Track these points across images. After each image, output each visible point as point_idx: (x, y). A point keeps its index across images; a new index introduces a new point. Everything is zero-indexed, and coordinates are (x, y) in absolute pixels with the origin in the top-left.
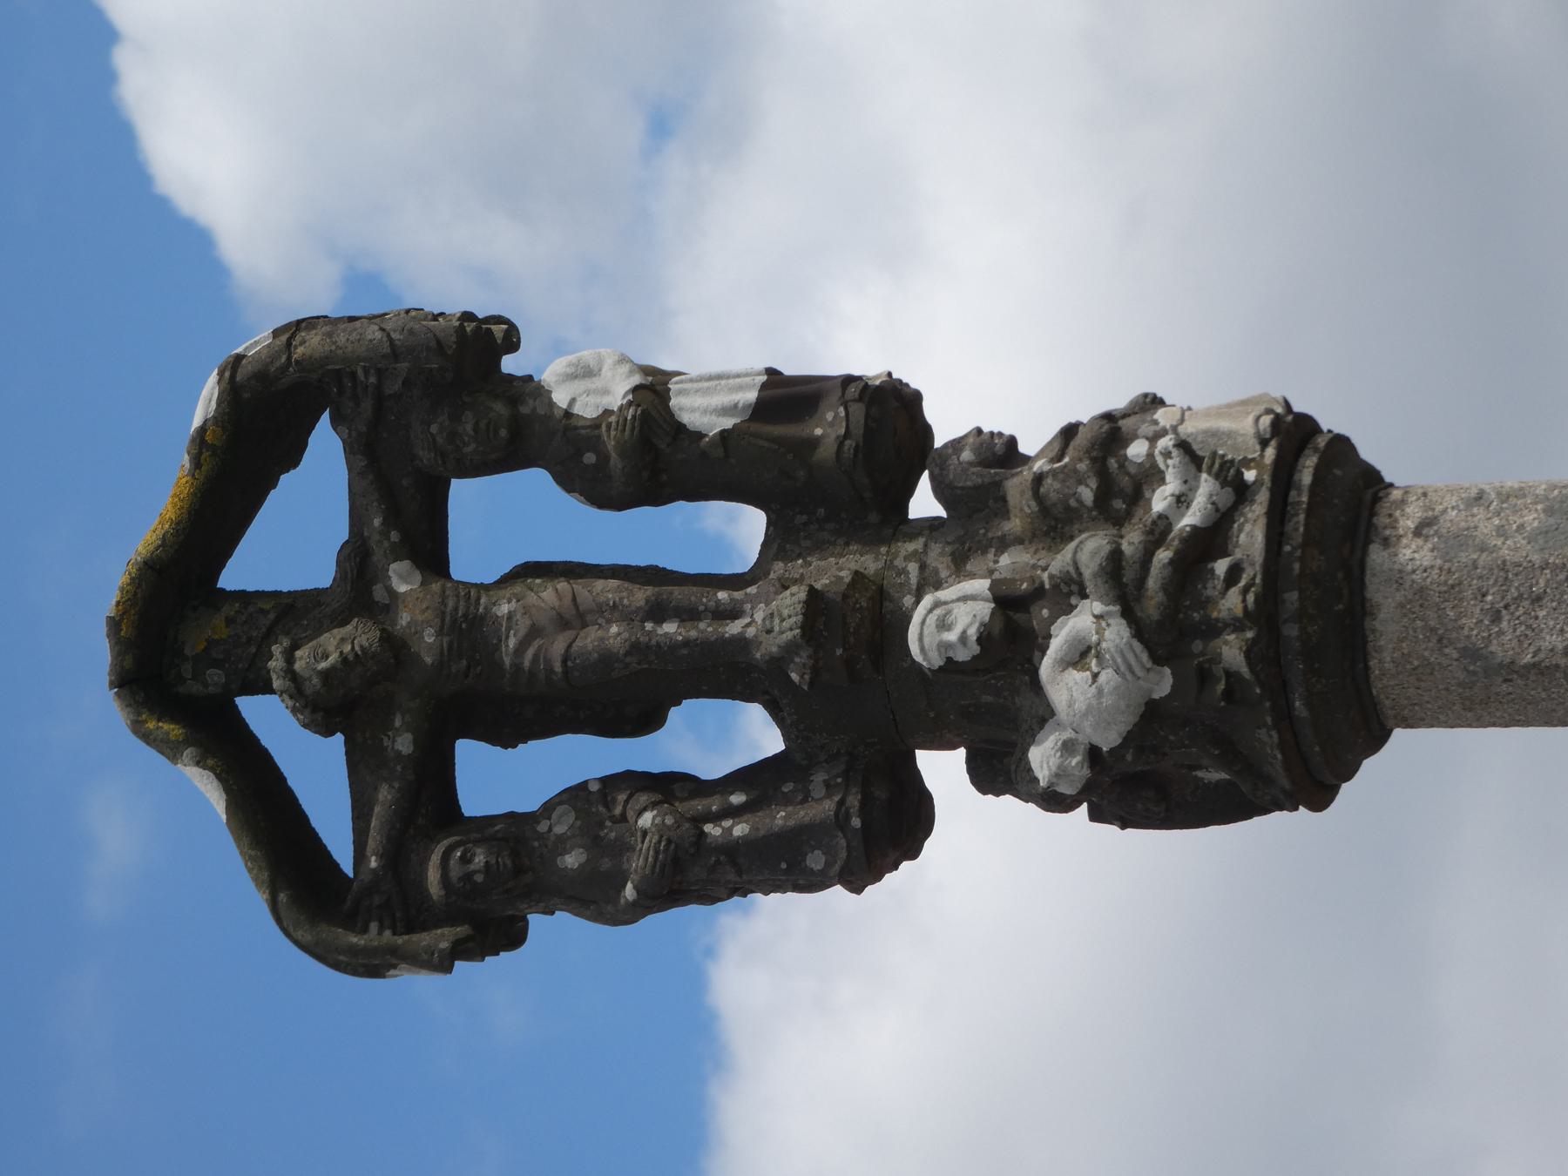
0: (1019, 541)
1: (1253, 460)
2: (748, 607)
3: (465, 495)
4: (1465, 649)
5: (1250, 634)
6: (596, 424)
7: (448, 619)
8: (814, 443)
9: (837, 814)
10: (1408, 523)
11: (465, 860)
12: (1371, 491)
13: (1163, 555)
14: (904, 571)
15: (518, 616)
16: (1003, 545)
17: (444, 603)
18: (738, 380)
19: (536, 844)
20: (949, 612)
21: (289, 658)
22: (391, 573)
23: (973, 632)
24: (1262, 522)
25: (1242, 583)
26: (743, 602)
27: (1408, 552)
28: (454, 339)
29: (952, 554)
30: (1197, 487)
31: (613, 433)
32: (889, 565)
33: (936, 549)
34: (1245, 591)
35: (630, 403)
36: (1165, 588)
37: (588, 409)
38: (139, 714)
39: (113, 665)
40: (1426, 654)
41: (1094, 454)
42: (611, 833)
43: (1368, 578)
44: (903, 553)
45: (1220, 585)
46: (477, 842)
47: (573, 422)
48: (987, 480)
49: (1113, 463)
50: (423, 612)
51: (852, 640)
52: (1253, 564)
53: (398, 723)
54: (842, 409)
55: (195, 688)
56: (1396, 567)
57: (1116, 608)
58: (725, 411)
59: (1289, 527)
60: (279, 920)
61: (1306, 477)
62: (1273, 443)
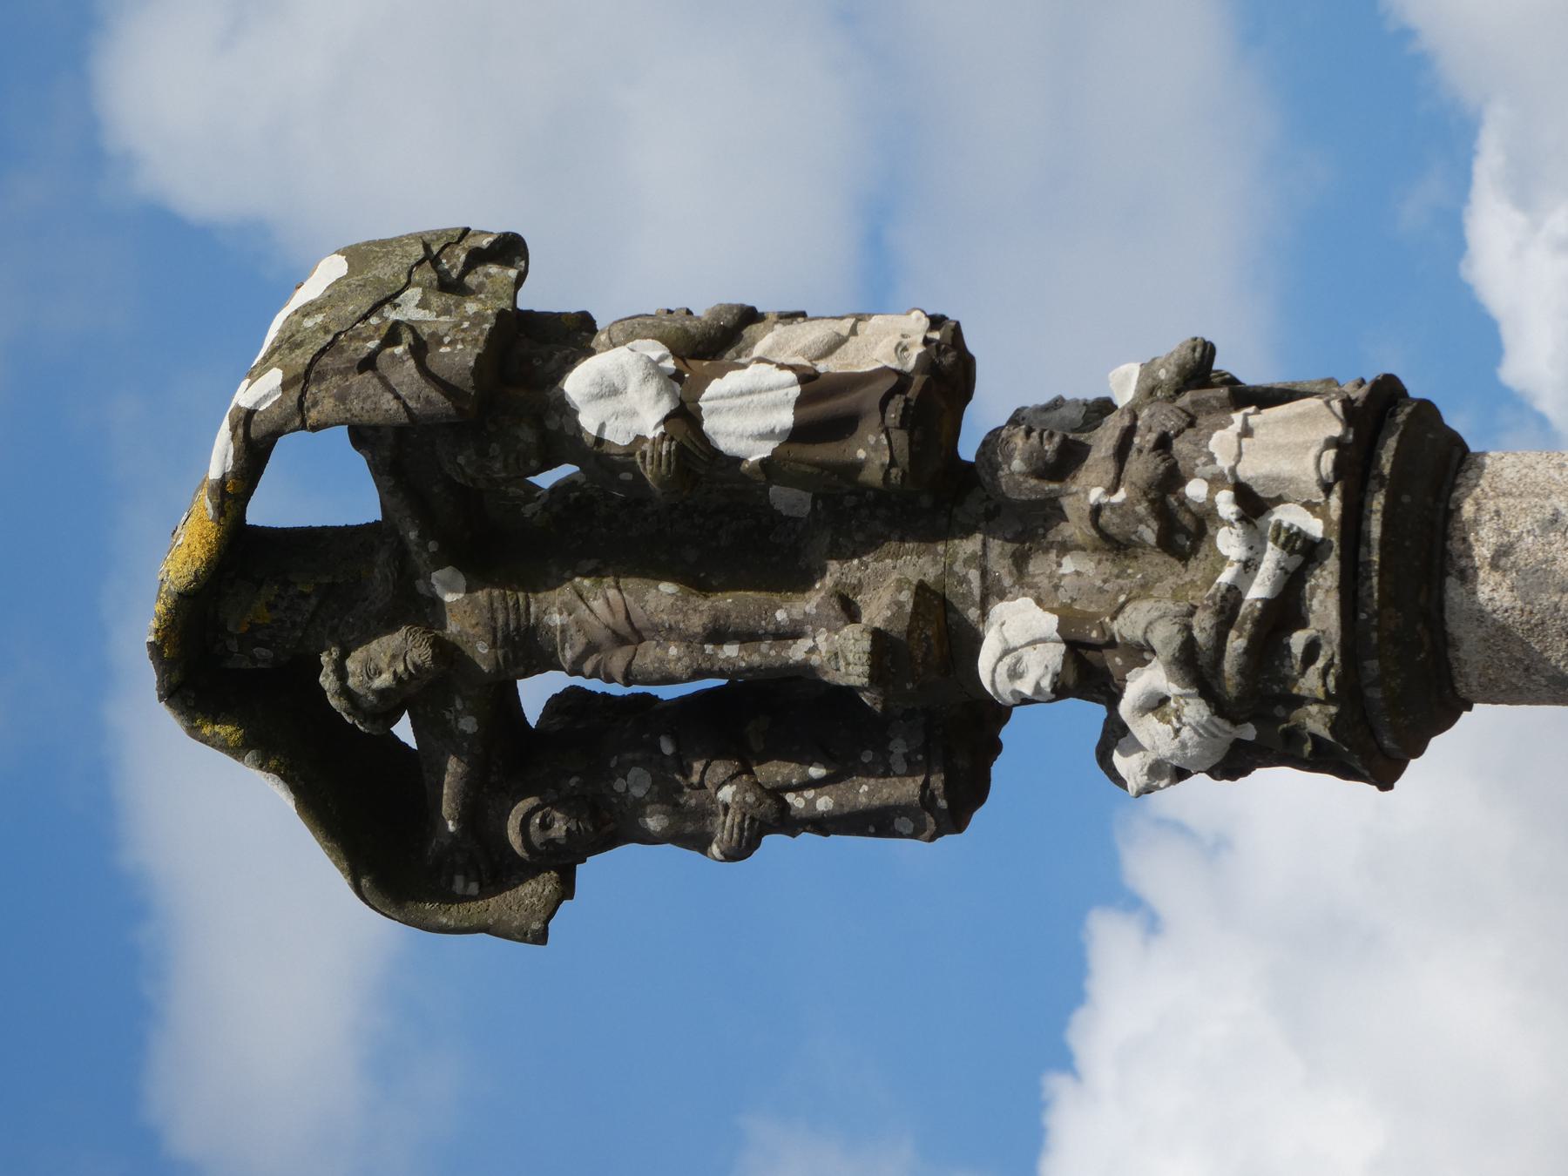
0: (1081, 548)
1: (1318, 504)
2: (809, 628)
3: (522, 684)
4: (1553, 677)
5: (1333, 710)
6: (630, 451)
7: (499, 635)
8: (858, 466)
9: (922, 798)
10: (1482, 552)
11: (545, 826)
13: (1236, 643)
14: (964, 580)
15: (573, 630)
16: (1065, 548)
17: (494, 619)
18: (771, 395)
19: (614, 800)
20: (1019, 660)
21: (341, 672)
22: (433, 581)
26: (801, 623)
28: (471, 383)
29: (1013, 555)
30: (1264, 551)
31: (649, 467)
32: (948, 571)
33: (995, 545)
34: (1324, 673)
35: (663, 435)
36: (1242, 672)
37: (619, 436)
38: (194, 720)
42: (691, 800)
43: (1447, 616)
44: (962, 556)
45: (1297, 667)
46: (556, 805)
47: (605, 449)
49: (1172, 499)
50: (474, 627)
52: (1330, 643)
53: (459, 705)
54: (883, 436)
55: (246, 664)
56: (1476, 607)
59: (1363, 593)
60: (367, 903)
61: (1375, 529)
62: (1337, 488)
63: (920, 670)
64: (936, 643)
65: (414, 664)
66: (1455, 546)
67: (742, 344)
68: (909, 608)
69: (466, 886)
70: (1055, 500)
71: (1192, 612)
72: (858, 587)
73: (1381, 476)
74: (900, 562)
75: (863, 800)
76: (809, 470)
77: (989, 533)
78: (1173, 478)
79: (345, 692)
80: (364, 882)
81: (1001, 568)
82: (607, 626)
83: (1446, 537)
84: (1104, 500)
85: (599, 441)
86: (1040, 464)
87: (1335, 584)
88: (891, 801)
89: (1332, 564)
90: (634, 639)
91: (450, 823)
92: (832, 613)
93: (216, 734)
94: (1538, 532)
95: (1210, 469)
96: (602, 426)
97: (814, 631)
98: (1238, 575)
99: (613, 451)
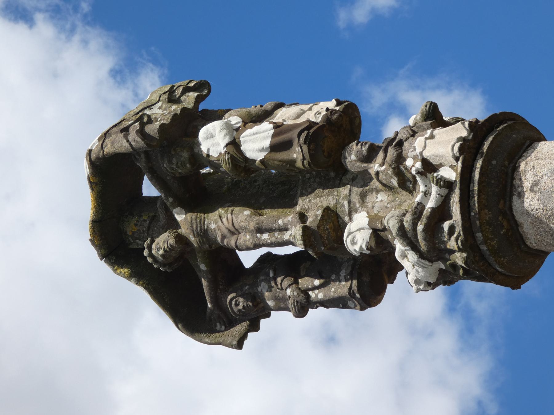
1: (455, 166)
2: (289, 226)
8: (293, 161)
9: (349, 293)
10: (527, 184)
12: (512, 165)
13: (420, 227)
14: (343, 205)
17: (192, 227)
18: (263, 134)
20: (354, 237)
23: (364, 246)
24: (458, 205)
25: (455, 235)
26: (287, 225)
27: (528, 201)
34: (457, 239)
36: (425, 239)
39: (98, 253)
40: (548, 241)
41: (393, 166)
43: (514, 213)
46: (242, 296)
48: (362, 169)
49: (402, 167)
51: (327, 242)
55: (136, 247)
57: (409, 248)
58: (262, 150)
59: (472, 204)
63: (327, 242)
64: (327, 232)
65: (170, 245)
66: (516, 182)
67: (272, 117)
68: (319, 218)
69: (221, 327)
70: (367, 171)
71: (404, 215)
72: (308, 210)
73: (483, 153)
74: (322, 199)
75: (332, 294)
76: (278, 163)
77: (352, 185)
78: (400, 159)
79: (151, 255)
80: (180, 326)
81: (356, 199)
82: (227, 228)
83: (513, 178)
84: (379, 169)
85: (208, 156)
86: (361, 156)
87: (458, 200)
88: (340, 295)
89: (457, 191)
90: (236, 232)
91: (209, 304)
92: (296, 220)
93: (121, 272)
94: (549, 174)
95: (414, 153)
96: (208, 150)
97: (291, 227)
98: (422, 198)
99: (213, 159)
